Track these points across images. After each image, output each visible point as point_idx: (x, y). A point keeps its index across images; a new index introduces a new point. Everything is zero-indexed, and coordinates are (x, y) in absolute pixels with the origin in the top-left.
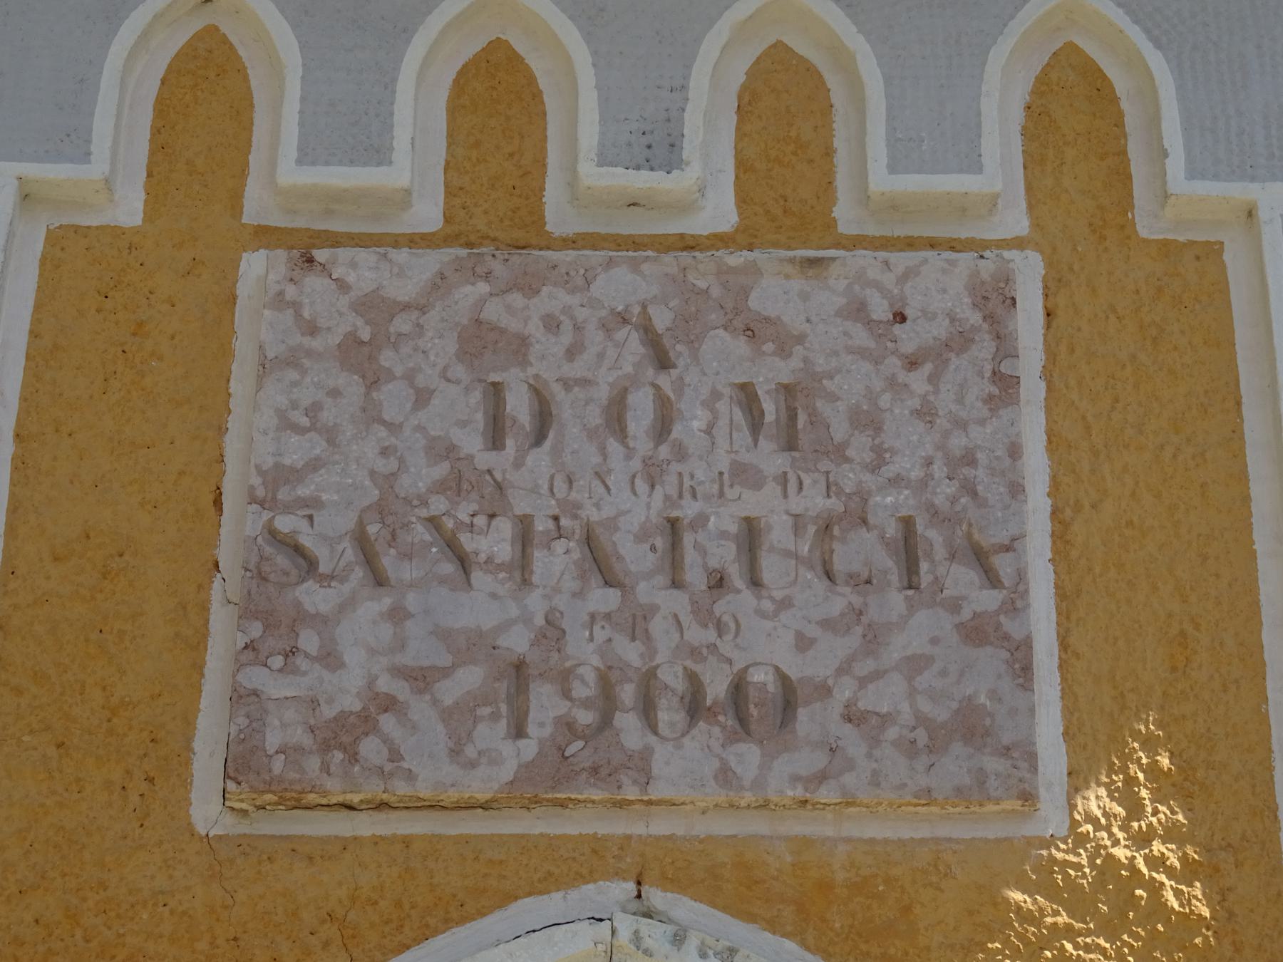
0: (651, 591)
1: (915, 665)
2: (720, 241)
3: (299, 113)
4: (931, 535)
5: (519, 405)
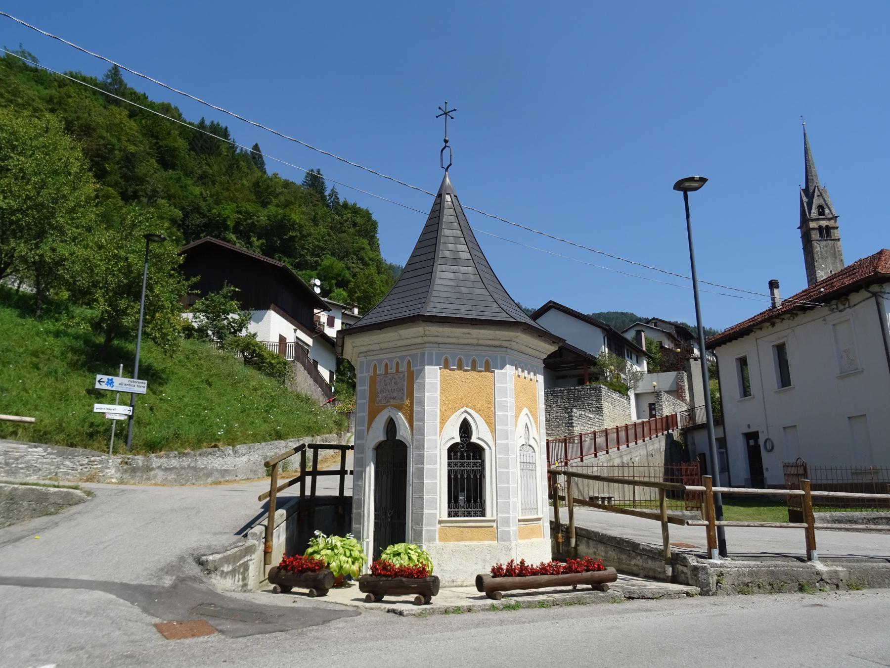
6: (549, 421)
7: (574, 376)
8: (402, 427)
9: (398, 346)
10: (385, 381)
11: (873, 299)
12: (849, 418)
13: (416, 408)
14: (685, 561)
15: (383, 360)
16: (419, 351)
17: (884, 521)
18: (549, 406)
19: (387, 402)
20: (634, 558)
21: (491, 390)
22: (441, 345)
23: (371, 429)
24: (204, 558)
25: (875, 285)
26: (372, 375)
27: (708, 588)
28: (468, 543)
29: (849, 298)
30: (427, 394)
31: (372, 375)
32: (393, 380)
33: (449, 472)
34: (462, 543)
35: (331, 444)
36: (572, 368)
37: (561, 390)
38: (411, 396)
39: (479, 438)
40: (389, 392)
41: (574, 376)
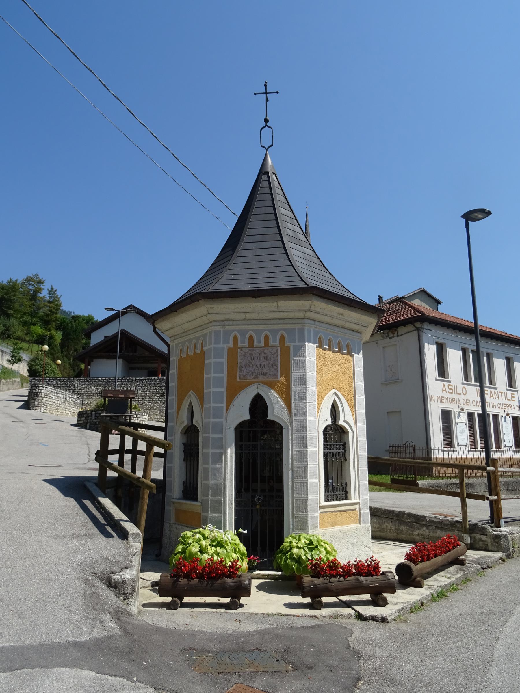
0: (259, 368)
1: (272, 372)
2: (263, 347)
3: (96, 454)
4: (273, 364)
5: (252, 358)
6: (142, 404)
7: (145, 368)
8: (276, 406)
9: (268, 318)
10: (251, 354)
11: (416, 332)
12: (388, 413)
13: (294, 387)
14: (484, 531)
15: (247, 331)
16: (297, 327)
17: (455, 485)
18: (143, 391)
19: (254, 378)
20: (418, 529)
21: (351, 373)
22: (317, 323)
23: (231, 406)
24: (116, 577)
25: (418, 322)
26: (232, 346)
27: (509, 552)
28: (340, 528)
29: (398, 329)
30: (308, 373)
31: (232, 346)
32: (263, 355)
33: (324, 453)
34: (337, 528)
35: (141, 423)
36: (145, 362)
37: (154, 379)
38: (287, 372)
39: (345, 421)
40: (257, 366)
41: (145, 368)
